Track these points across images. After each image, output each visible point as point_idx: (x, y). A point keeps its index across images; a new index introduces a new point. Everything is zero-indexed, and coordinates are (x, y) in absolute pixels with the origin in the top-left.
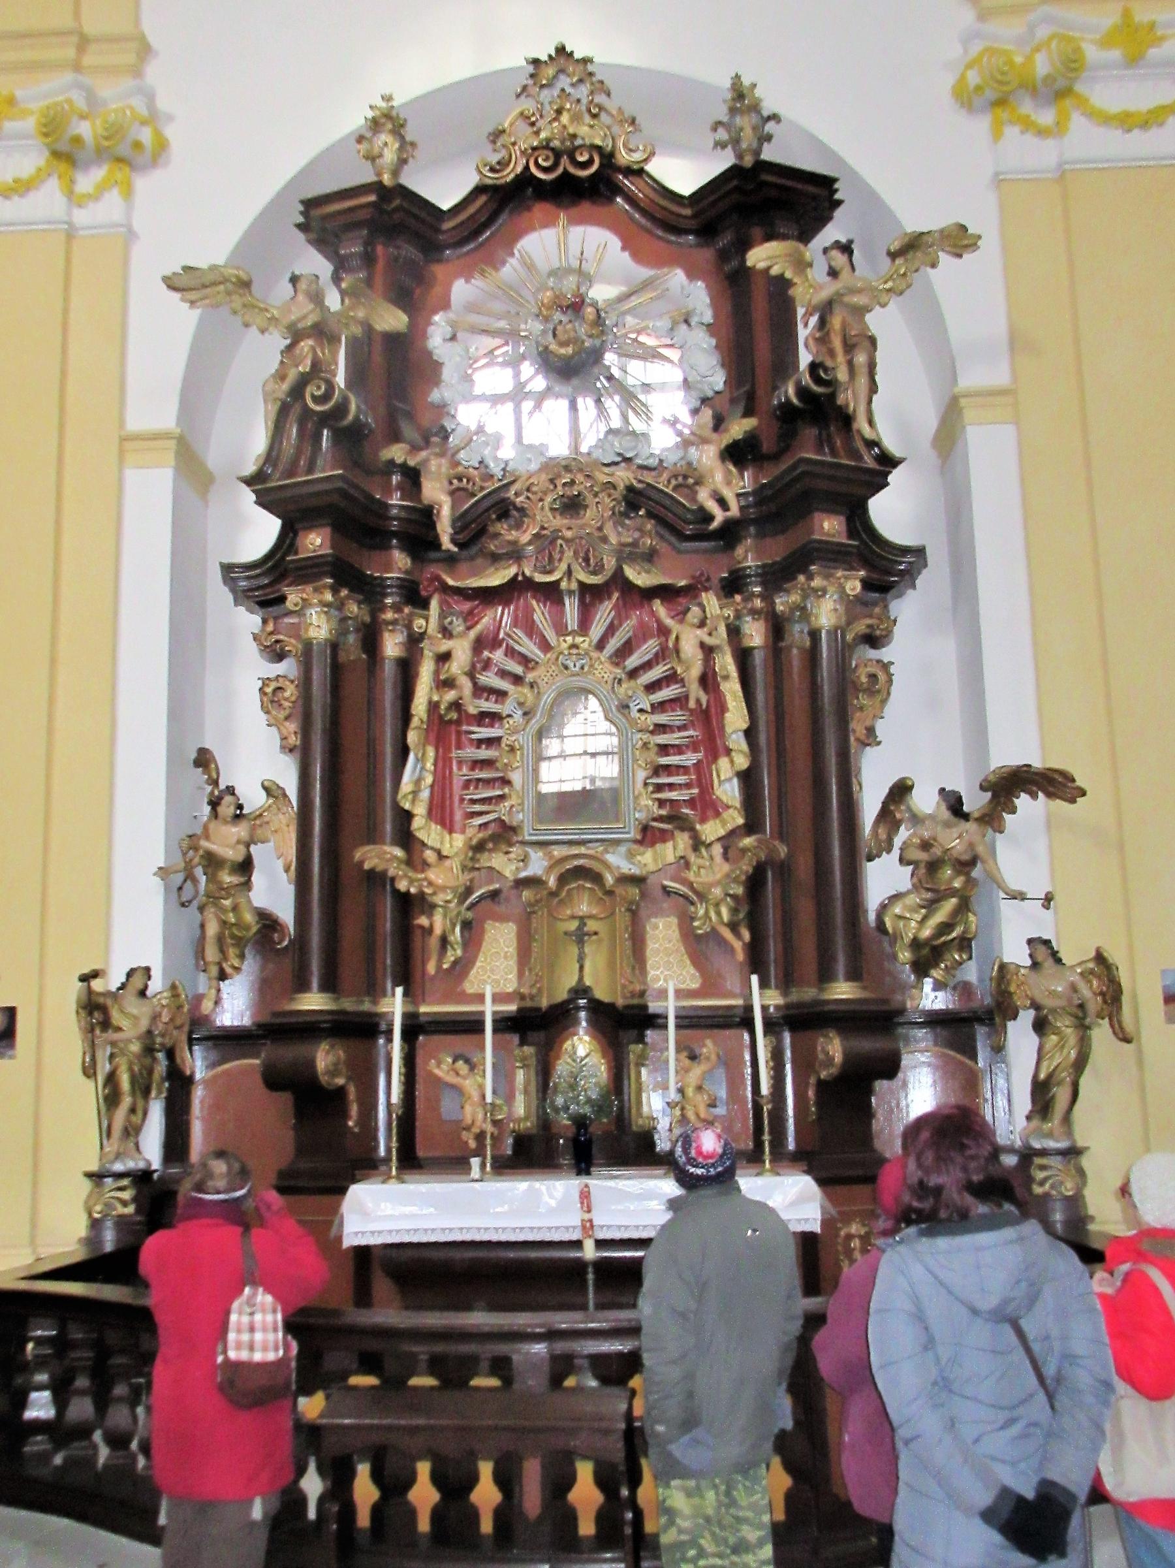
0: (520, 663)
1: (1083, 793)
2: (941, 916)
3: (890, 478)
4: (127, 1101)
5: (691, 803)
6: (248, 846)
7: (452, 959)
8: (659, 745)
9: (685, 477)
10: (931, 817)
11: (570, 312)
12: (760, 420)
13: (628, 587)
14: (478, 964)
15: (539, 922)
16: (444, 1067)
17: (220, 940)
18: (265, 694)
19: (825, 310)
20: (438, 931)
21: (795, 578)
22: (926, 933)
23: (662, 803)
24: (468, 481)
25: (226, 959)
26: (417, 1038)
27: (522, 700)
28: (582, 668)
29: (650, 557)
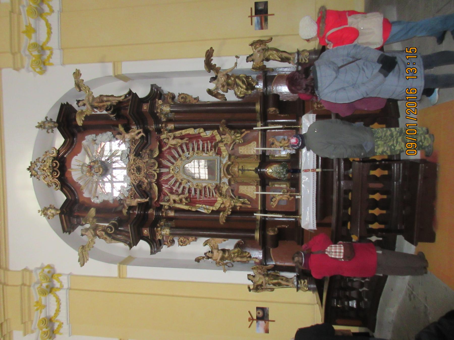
0: (177, 183)
1: (212, 48)
3: (134, 93)
4: (280, 281)
5: (211, 143)
6: (219, 250)
9: (133, 142)
10: (216, 85)
13: (159, 156)
14: (249, 195)
16: (274, 204)
19: (93, 107)
20: (241, 205)
22: (244, 87)
23: (211, 150)
25: (246, 256)
27: (185, 183)
28: (178, 168)
29: (152, 151)
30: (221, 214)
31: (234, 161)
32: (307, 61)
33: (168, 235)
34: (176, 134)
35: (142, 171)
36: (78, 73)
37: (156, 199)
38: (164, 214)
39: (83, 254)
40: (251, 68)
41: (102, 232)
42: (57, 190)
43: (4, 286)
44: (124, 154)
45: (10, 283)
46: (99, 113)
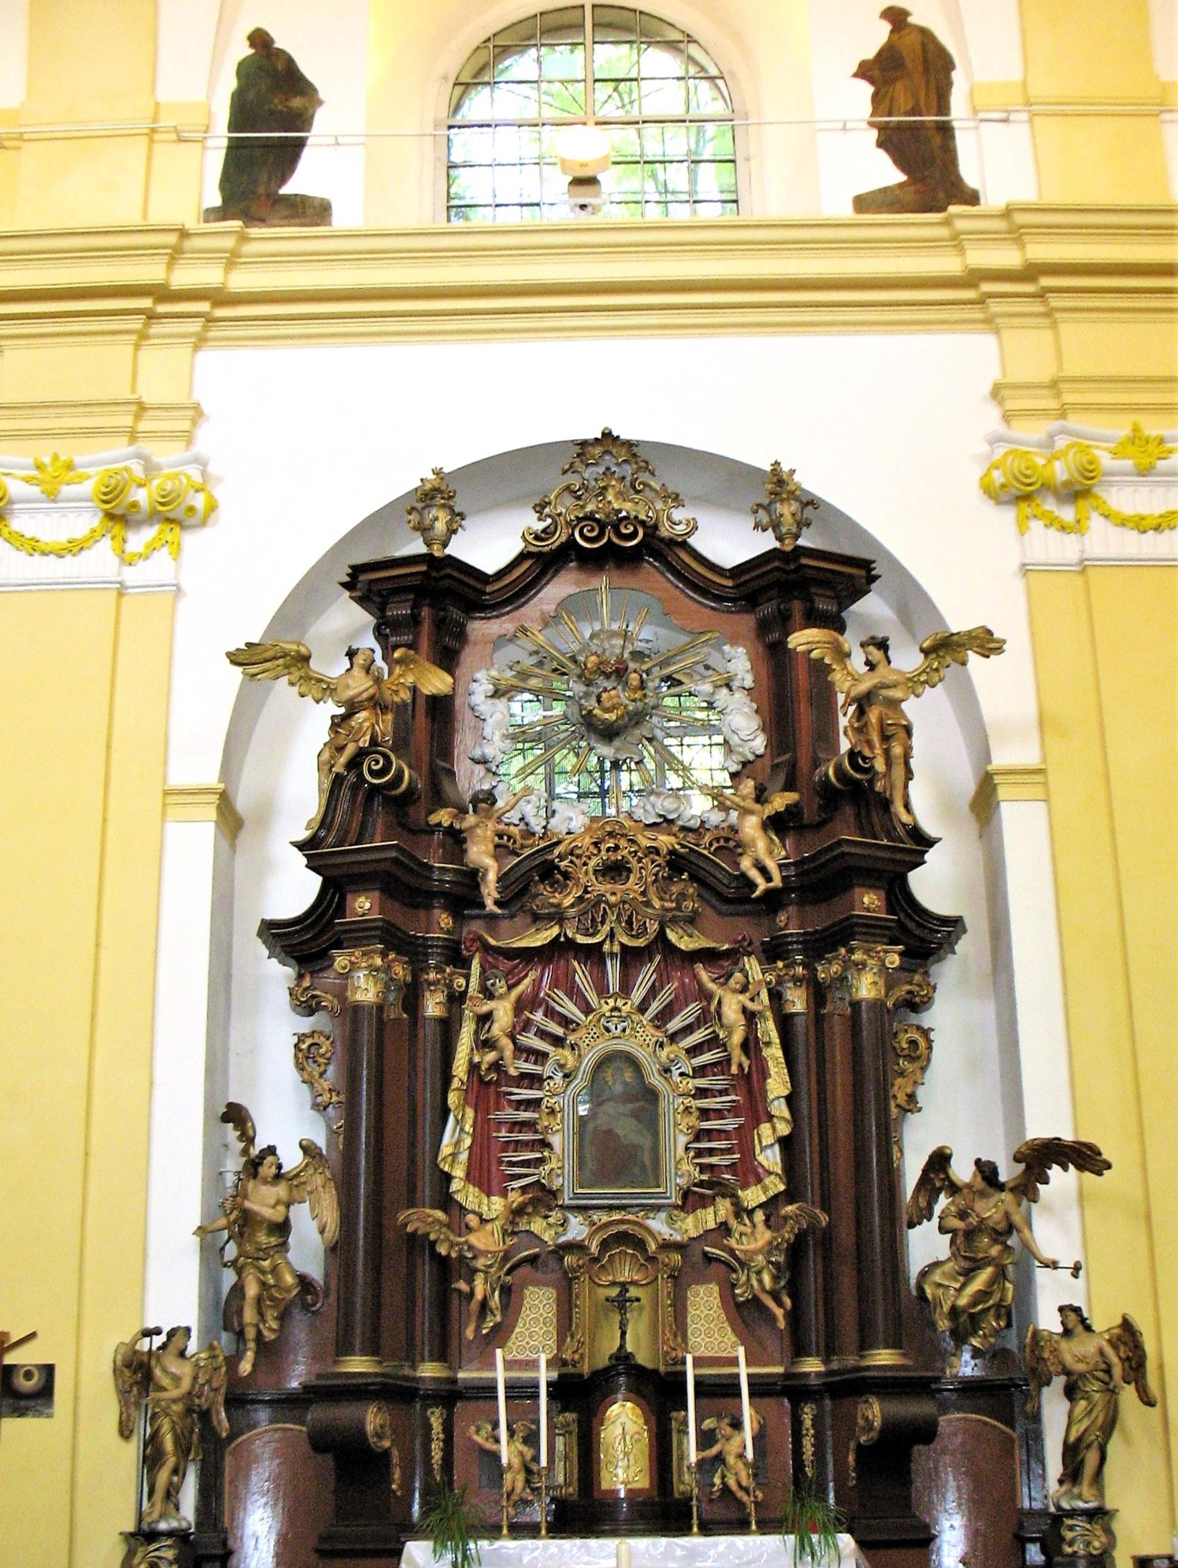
0: (560, 1024)
1: (1109, 1166)
2: (979, 1282)
3: (927, 857)
4: (171, 1461)
5: (732, 1168)
6: (288, 1206)
7: (491, 1324)
8: (699, 1109)
9: (727, 840)
10: (969, 1186)
11: (613, 677)
12: (802, 794)
13: (670, 949)
14: (517, 1330)
15: (583, 1288)
16: (483, 1433)
17: (259, 1300)
18: (301, 1050)
19: (863, 703)
20: (479, 1295)
21: (836, 950)
22: (963, 1301)
23: (703, 1168)
24: (509, 840)
25: (264, 1322)
26: (455, 1404)
27: (562, 1062)
28: (624, 1030)
29: (692, 920)
30: (439, 1214)
31: (661, 1266)
32: (1068, 1550)
33: (349, 993)
34: (766, 1019)
35: (609, 886)
36: (992, 645)
37: (492, 942)
38: (432, 976)
39: (275, 658)
40: (1041, 1327)
41: (368, 737)
42: (525, 540)
43: (134, 337)
44: (675, 806)
45: (144, 354)
46: (843, 722)
